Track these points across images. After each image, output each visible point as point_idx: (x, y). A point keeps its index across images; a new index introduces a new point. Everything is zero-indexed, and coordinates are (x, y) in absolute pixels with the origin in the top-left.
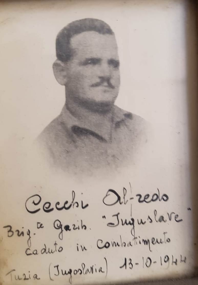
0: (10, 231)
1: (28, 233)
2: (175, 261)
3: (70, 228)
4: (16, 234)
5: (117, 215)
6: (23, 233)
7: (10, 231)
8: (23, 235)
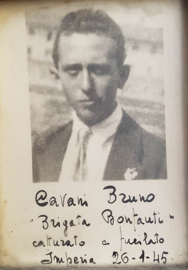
1: (65, 224)
3: (136, 199)
4: (50, 224)
6: (58, 224)
7: (113, 194)
8: (59, 226)
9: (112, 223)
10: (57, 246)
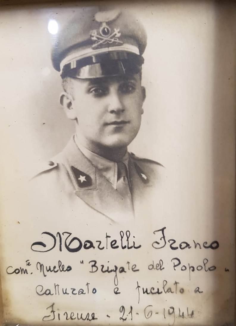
0: (94, 266)
2: (181, 314)
4: (100, 268)
5: (163, 230)
7: (94, 266)
9: (122, 233)
10: (66, 294)
